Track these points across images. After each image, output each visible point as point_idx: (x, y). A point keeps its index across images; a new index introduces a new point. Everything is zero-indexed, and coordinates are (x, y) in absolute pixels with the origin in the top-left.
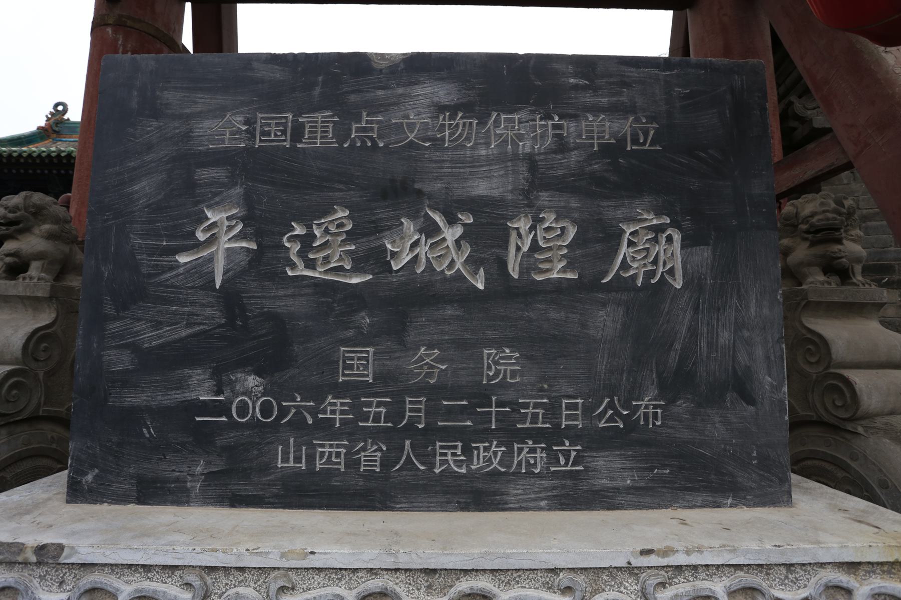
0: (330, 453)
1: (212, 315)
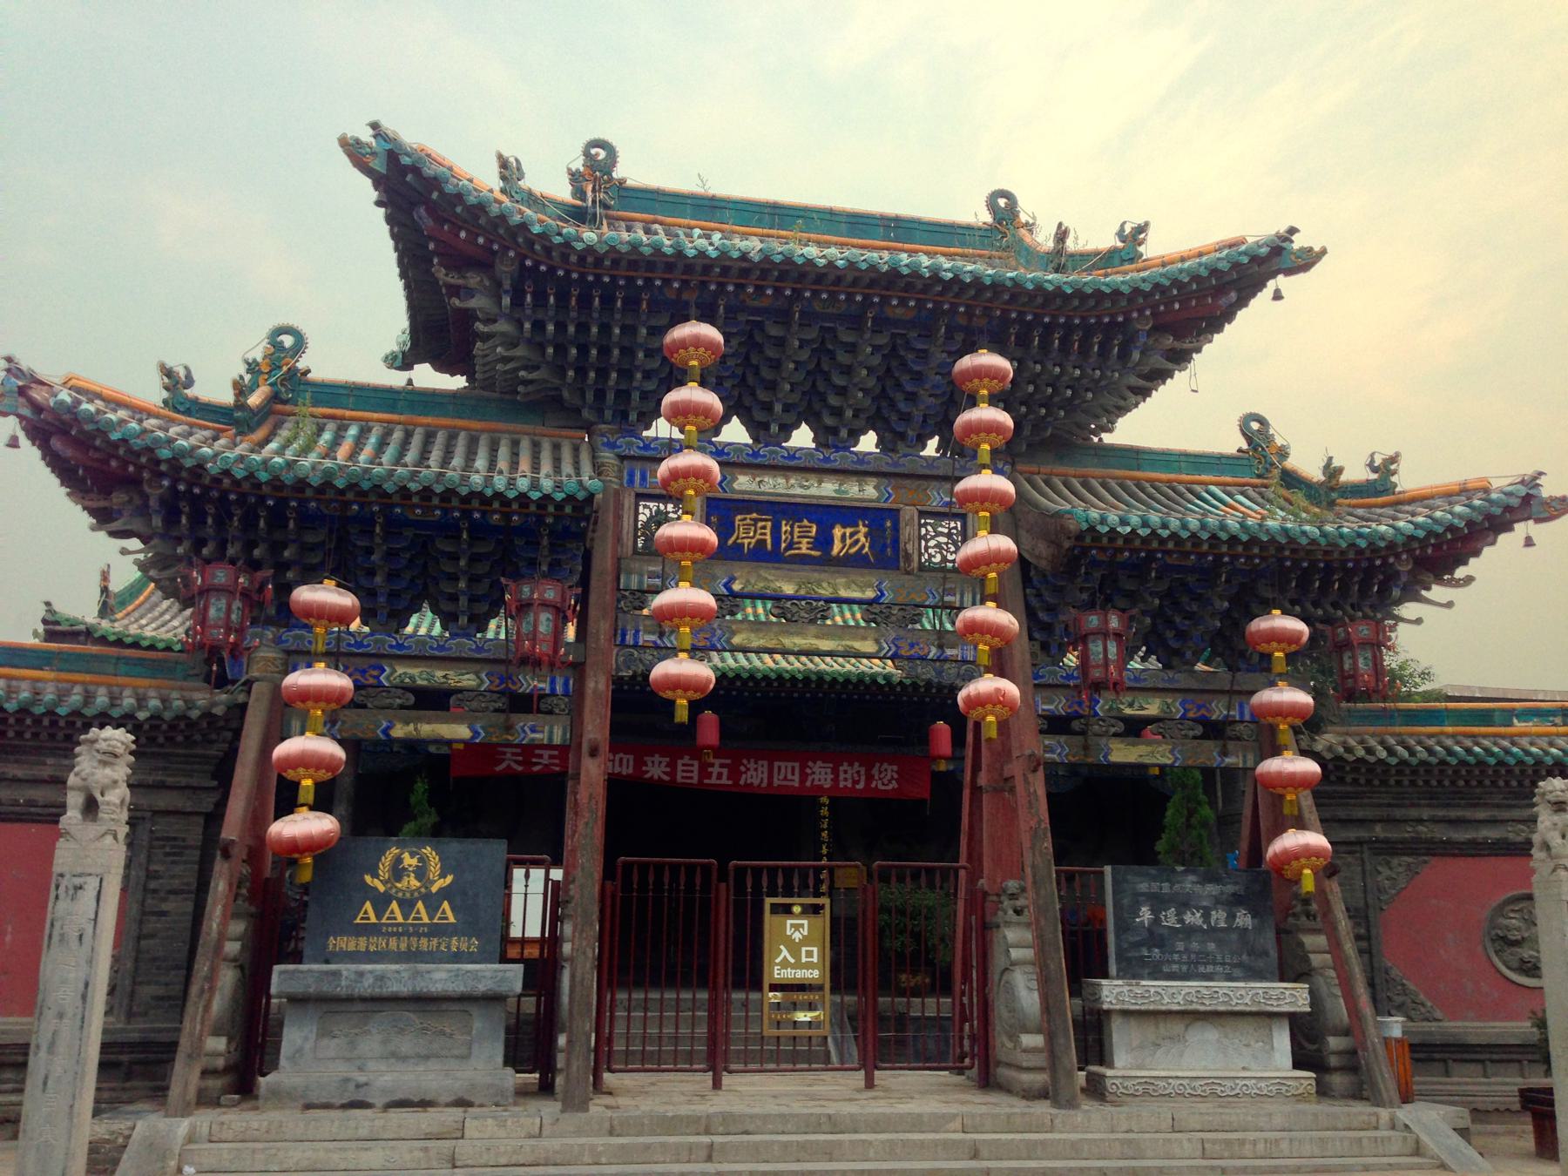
0: (1175, 967)
1: (1145, 934)
